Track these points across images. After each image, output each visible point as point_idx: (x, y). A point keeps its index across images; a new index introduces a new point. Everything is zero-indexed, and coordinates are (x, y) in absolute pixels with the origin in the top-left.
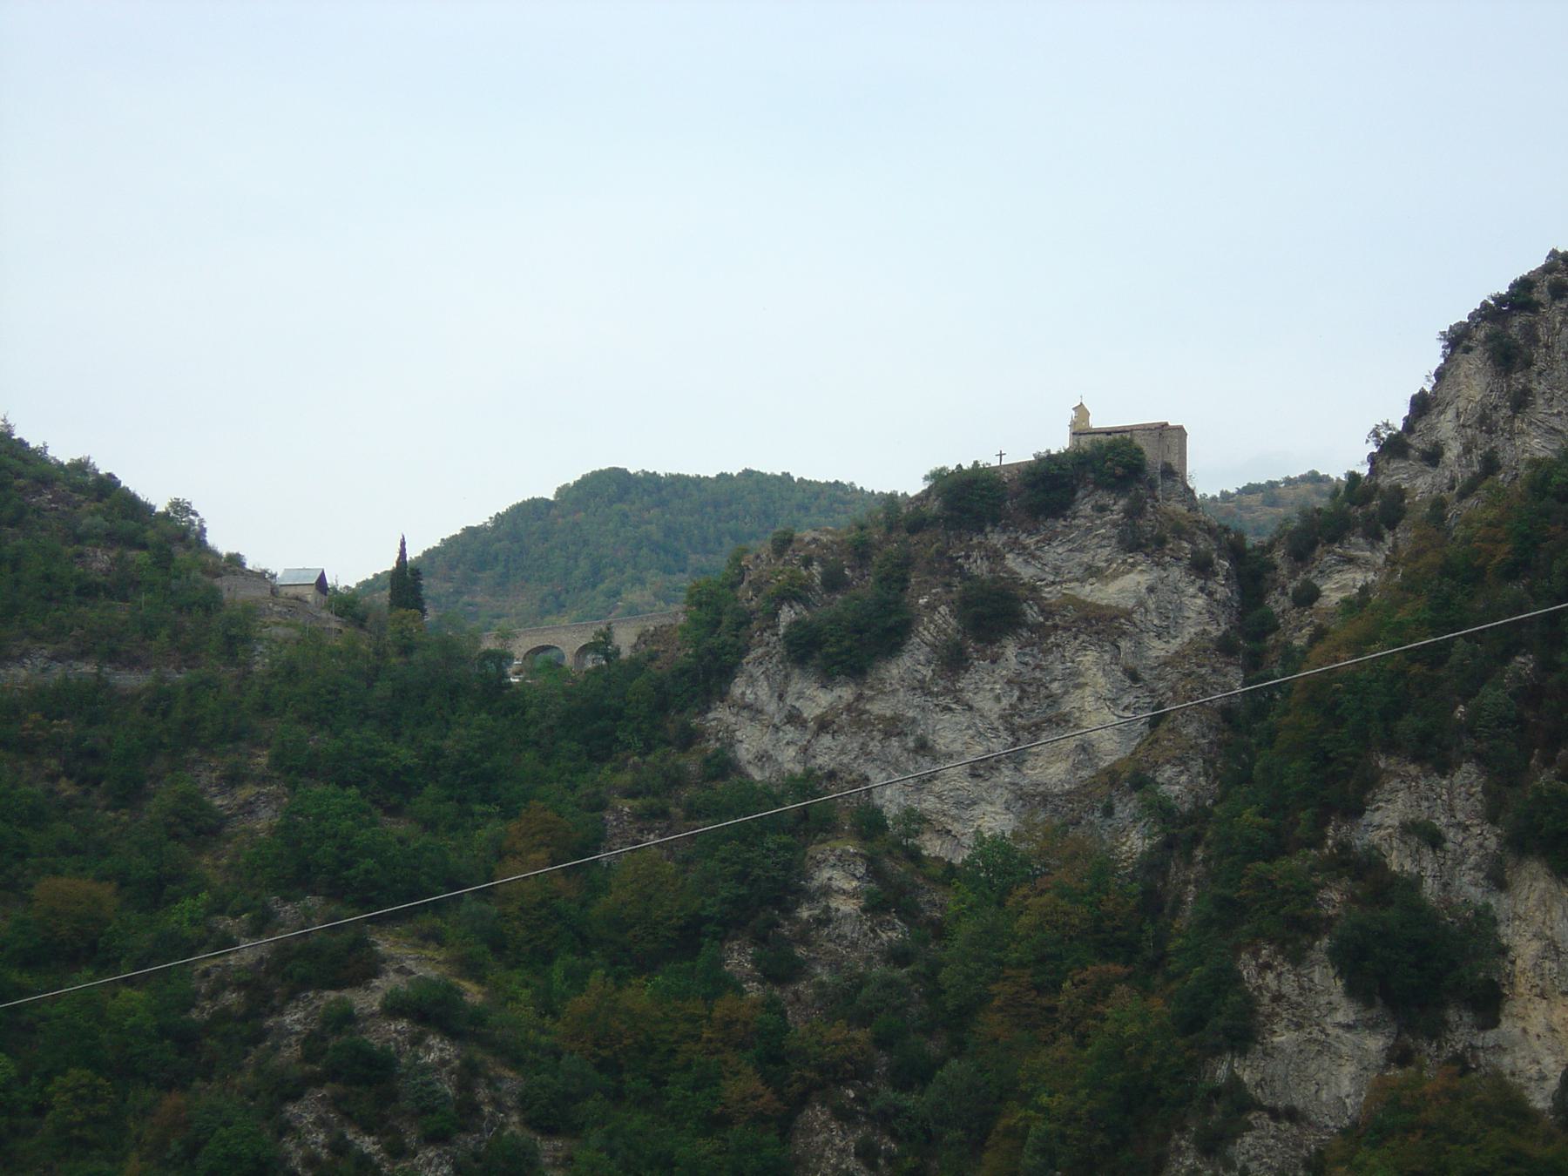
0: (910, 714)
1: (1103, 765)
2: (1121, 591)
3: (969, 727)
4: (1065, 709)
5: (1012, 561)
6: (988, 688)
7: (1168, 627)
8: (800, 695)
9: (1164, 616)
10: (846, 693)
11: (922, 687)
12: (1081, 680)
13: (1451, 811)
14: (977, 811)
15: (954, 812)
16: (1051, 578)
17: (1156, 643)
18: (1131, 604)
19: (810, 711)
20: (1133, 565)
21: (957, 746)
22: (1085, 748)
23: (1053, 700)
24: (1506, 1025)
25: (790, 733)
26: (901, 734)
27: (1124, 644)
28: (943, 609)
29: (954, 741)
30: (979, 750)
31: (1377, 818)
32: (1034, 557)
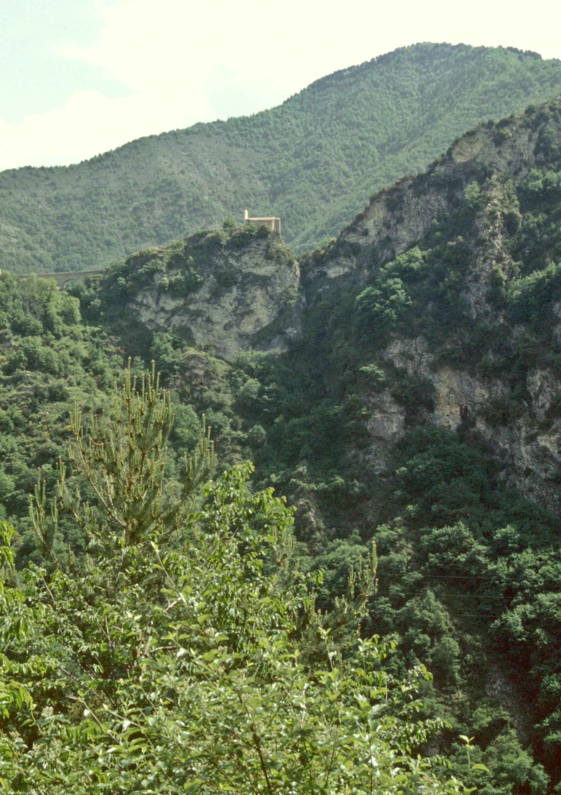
4: (252, 308)
5: (232, 261)
6: (228, 301)
8: (165, 302)
9: (281, 280)
10: (181, 302)
11: (208, 301)
13: (416, 350)
14: (225, 340)
18: (270, 275)
21: (219, 320)
22: (258, 320)
23: (248, 305)
24: (436, 412)
25: (162, 314)
26: (202, 316)
27: (269, 289)
28: (212, 276)
30: (226, 321)
31: (391, 351)
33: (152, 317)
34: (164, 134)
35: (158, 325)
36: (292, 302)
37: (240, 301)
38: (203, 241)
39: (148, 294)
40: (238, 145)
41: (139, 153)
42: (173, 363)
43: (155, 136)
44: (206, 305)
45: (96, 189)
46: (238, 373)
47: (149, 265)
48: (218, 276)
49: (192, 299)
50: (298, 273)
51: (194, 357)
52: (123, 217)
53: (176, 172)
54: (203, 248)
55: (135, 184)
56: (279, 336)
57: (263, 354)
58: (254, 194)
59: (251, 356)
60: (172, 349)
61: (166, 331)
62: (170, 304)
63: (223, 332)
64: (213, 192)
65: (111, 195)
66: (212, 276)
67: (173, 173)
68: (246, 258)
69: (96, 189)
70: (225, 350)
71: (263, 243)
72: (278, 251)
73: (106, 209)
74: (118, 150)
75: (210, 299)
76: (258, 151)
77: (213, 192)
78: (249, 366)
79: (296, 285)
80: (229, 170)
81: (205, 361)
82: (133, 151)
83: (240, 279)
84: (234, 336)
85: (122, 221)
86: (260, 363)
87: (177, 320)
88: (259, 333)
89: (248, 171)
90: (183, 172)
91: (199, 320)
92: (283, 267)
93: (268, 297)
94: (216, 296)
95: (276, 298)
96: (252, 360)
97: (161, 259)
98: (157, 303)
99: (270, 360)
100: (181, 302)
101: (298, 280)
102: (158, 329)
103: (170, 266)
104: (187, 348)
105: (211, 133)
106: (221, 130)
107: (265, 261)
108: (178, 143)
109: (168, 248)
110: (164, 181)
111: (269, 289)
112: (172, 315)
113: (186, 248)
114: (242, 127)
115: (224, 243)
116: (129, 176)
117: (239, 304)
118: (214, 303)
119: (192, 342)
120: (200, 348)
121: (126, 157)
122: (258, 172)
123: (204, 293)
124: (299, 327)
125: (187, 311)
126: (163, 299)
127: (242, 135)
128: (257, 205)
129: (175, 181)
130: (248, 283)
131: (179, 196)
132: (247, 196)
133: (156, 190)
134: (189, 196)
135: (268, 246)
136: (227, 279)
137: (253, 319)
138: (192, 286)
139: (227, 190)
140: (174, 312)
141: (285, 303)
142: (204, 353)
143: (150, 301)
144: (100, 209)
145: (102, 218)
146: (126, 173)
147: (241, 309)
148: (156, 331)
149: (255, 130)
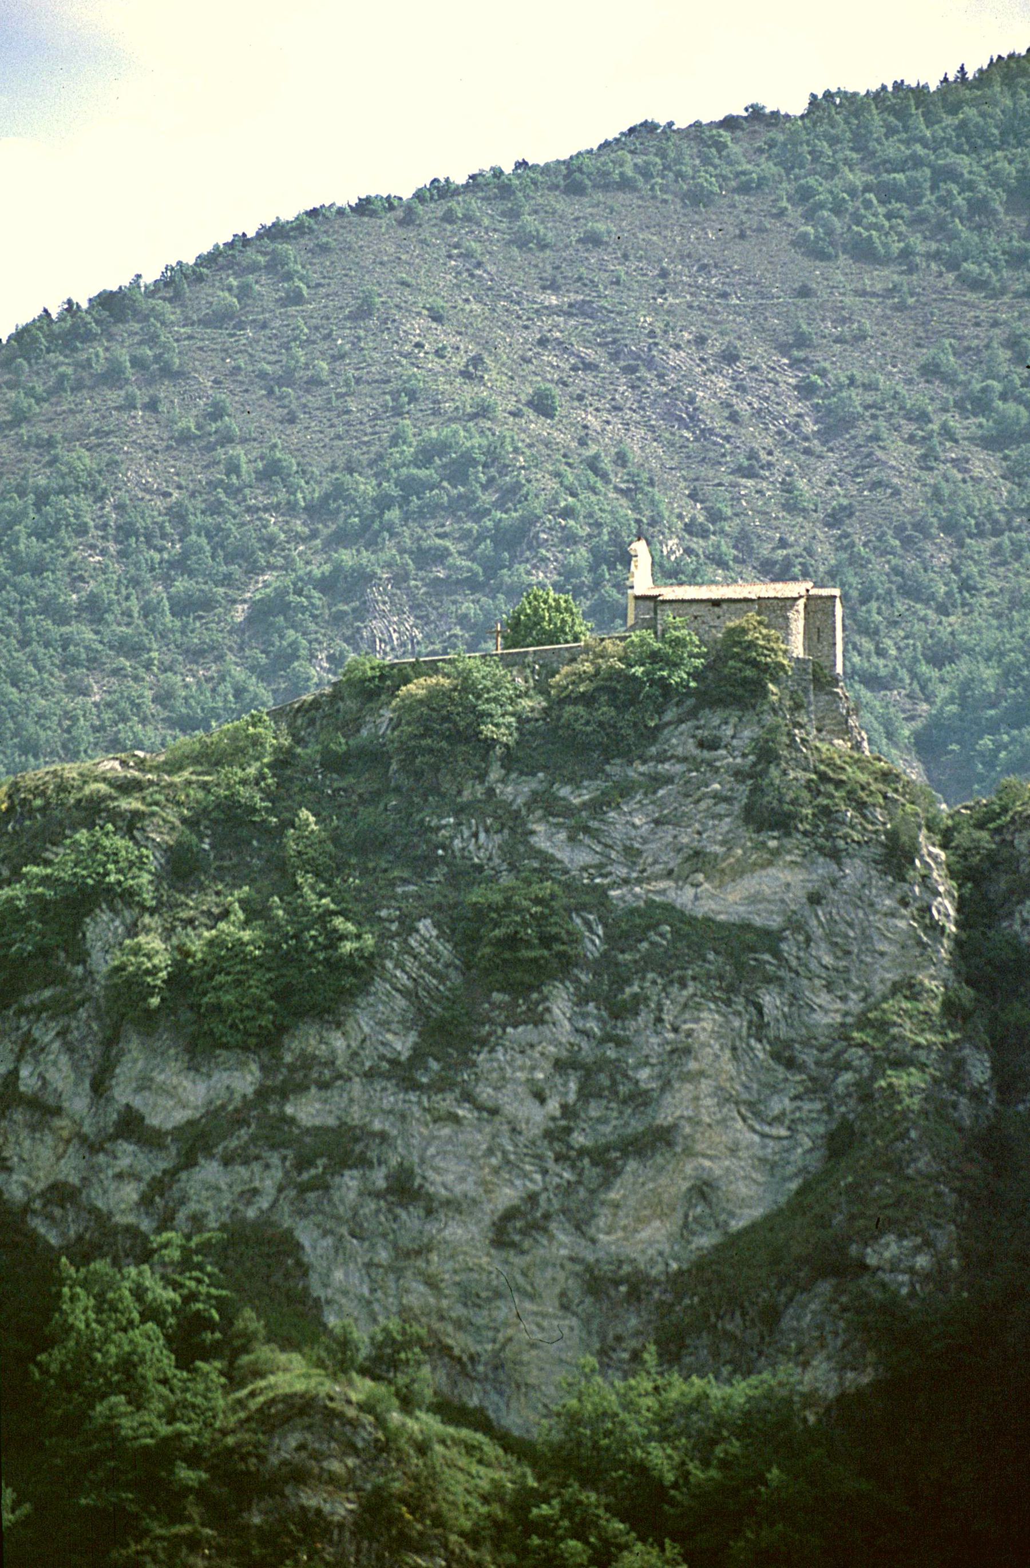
0: (377, 1126)
1: (736, 1225)
2: (754, 899)
3: (490, 1152)
4: (665, 1117)
5: (547, 837)
6: (522, 1070)
7: (847, 970)
8: (144, 1084)
10: (243, 1080)
11: (402, 1073)
12: (693, 1065)
14: (503, 1311)
15: (459, 1311)
16: (623, 872)
17: (824, 998)
18: (775, 922)
19: (165, 1115)
20: (776, 853)
21: (469, 1187)
25: (127, 1154)
26: (364, 1163)
28: (425, 927)
29: (462, 1179)
30: (508, 1195)
32: (586, 830)
33: (69, 1170)
34: (440, 190)
35: (101, 1218)
36: (901, 1080)
37: (594, 1076)
38: (381, 723)
39: (45, 1033)
40: (864, 253)
41: (296, 298)
42: (169, 1450)
43: (390, 203)
44: (390, 1098)
45: (42, 498)
46: (568, 1509)
47: (62, 863)
48: (465, 928)
49: (307, 1061)
50: (945, 908)
51: (301, 1408)
52: (196, 655)
53: (503, 406)
54: (382, 763)
55: (271, 472)
56: (825, 1287)
57: (731, 1393)
58: (949, 527)
59: (642, 1400)
60: (167, 1361)
61: (145, 1255)
62: (179, 1093)
63: (487, 1259)
64: (715, 516)
65: (126, 531)
66: (425, 927)
67: (483, 411)
68: (632, 820)
69: (42, 498)
70: (501, 1371)
71: (738, 734)
72: (825, 779)
73: (94, 609)
74: (177, 281)
75: (418, 1056)
76: (977, 284)
77: (715, 516)
78: (641, 1469)
79: (932, 982)
80: (806, 390)
81: (368, 1432)
82: (262, 286)
83: (594, 945)
84: (554, 1281)
85: (185, 681)
86: (704, 1447)
87: (211, 1188)
88: (702, 1272)
89: (920, 395)
90: (542, 405)
91: (349, 1184)
92: (853, 871)
93: (760, 1051)
94: (449, 1037)
95: (808, 1057)
96: (665, 1426)
97: (131, 825)
98: (99, 1087)
99: (768, 1428)
100: (243, 1080)
101: (944, 951)
102: (105, 1241)
103: (181, 869)
104: (264, 1352)
105: (708, 181)
106: (769, 168)
107: (747, 836)
108: (522, 241)
109: (174, 766)
110: (426, 455)
111: (771, 1000)
112: (188, 1162)
113: (283, 761)
114: (892, 149)
115: (500, 730)
116: (233, 424)
117: (585, 1094)
118: (441, 1085)
119: (299, 1322)
120: (340, 1358)
121: (219, 319)
122: (980, 404)
123: (377, 1026)
124: (945, 1237)
125: (278, 1133)
126: (134, 1058)
127: (888, 193)
128: (966, 586)
129: (493, 456)
130: (643, 966)
131: (516, 540)
132: (912, 535)
133: (383, 503)
134: (570, 539)
135: (767, 753)
136: (512, 941)
137: (675, 1181)
138: (307, 985)
139: (792, 506)
140: (196, 1141)
141: (865, 1093)
142: (362, 1389)
143: (59, 1074)
144: (52, 609)
145: (69, 663)
146: (217, 412)
147: (602, 1124)
148: (83, 1253)
149: (964, 163)
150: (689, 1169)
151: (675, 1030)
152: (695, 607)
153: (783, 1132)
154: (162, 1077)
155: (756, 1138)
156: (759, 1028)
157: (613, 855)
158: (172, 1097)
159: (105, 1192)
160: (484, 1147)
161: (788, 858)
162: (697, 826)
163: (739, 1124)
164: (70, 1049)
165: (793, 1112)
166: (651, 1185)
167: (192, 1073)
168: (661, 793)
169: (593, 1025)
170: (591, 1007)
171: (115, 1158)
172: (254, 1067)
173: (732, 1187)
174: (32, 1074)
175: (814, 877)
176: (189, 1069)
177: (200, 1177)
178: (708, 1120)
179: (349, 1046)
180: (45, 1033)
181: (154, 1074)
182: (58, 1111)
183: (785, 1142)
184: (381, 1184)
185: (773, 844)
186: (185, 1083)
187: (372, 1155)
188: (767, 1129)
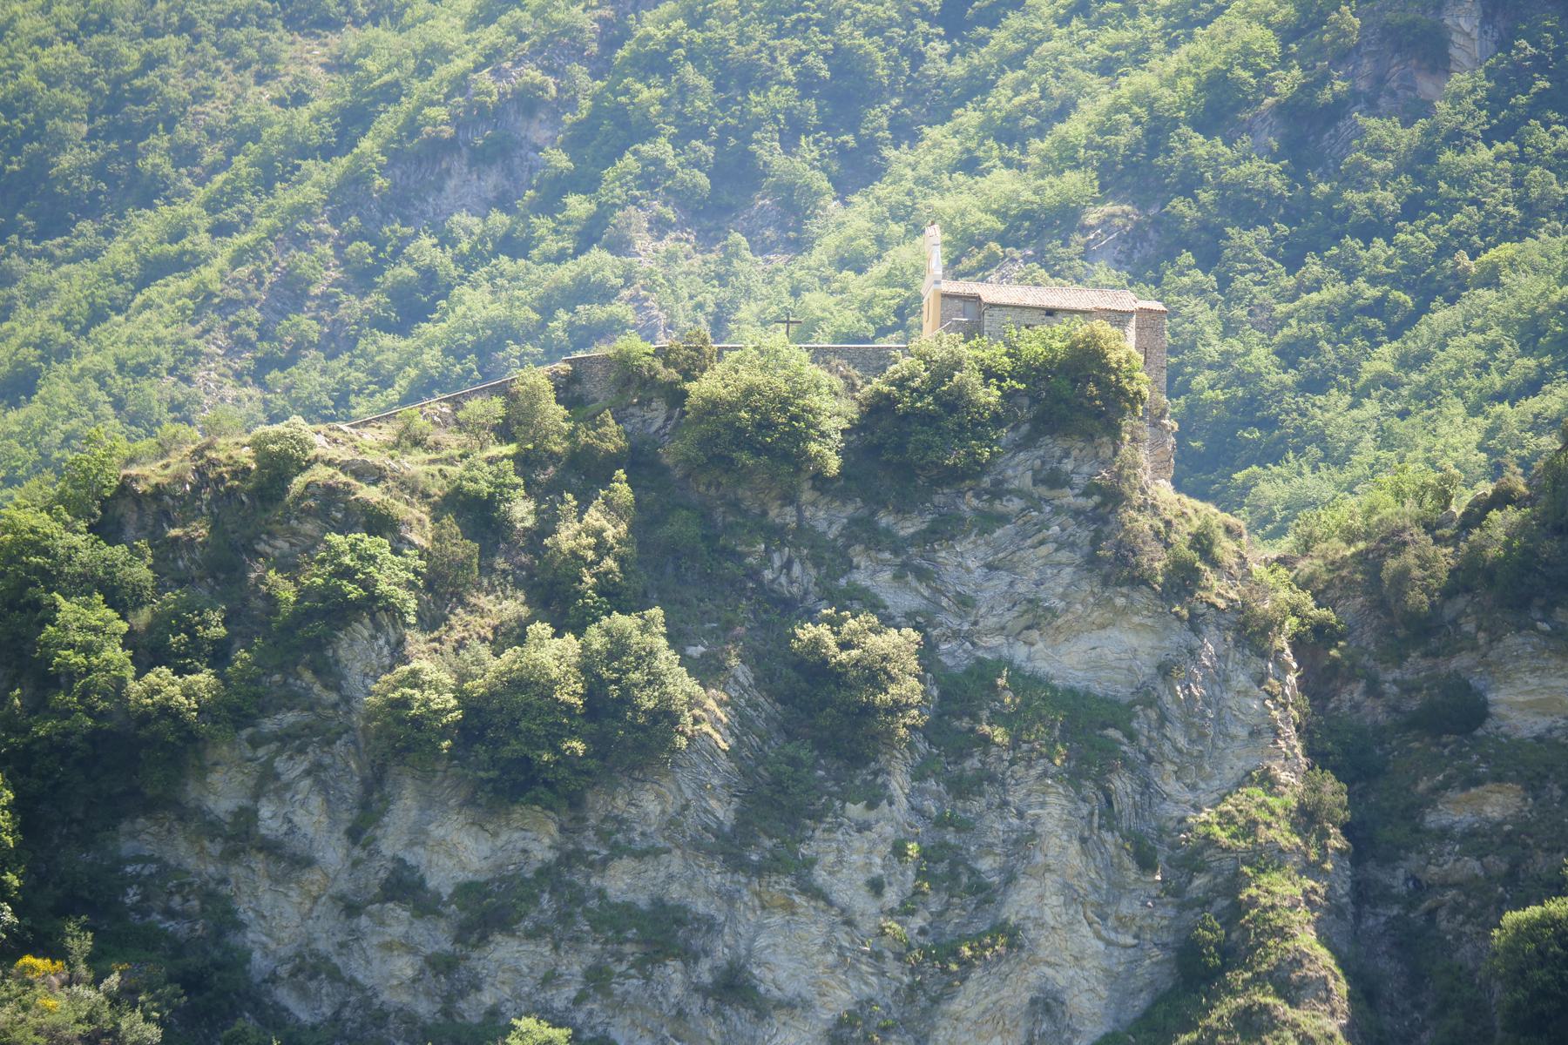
6: (862, 853)
18: (1124, 693)
19: (442, 876)
33: (325, 935)
39: (291, 768)
62: (458, 850)
111: (1121, 784)
118: (773, 865)
126: (405, 807)
150: (1032, 977)
151: (1020, 815)
152: (1027, 314)
153: (1130, 941)
154: (441, 832)
155: (1101, 946)
156: (1109, 814)
157: (944, 602)
158: (451, 856)
159: (368, 962)
160: (820, 941)
161: (1136, 619)
162: (1035, 575)
163: (1085, 930)
164: (323, 787)
165: (1143, 918)
166: (994, 997)
167: (475, 829)
168: (998, 533)
169: (931, 806)
170: (931, 784)
171: (382, 923)
172: (553, 828)
173: (1076, 1000)
174: (274, 816)
175: (1167, 643)
176: (473, 824)
177: (496, 955)
178: (1052, 923)
179: (663, 812)
180: (291, 768)
181: (432, 827)
182: (307, 862)
183: (1130, 951)
184: (707, 978)
185: (1120, 601)
186: (467, 842)
187: (697, 942)
188: (1113, 936)
